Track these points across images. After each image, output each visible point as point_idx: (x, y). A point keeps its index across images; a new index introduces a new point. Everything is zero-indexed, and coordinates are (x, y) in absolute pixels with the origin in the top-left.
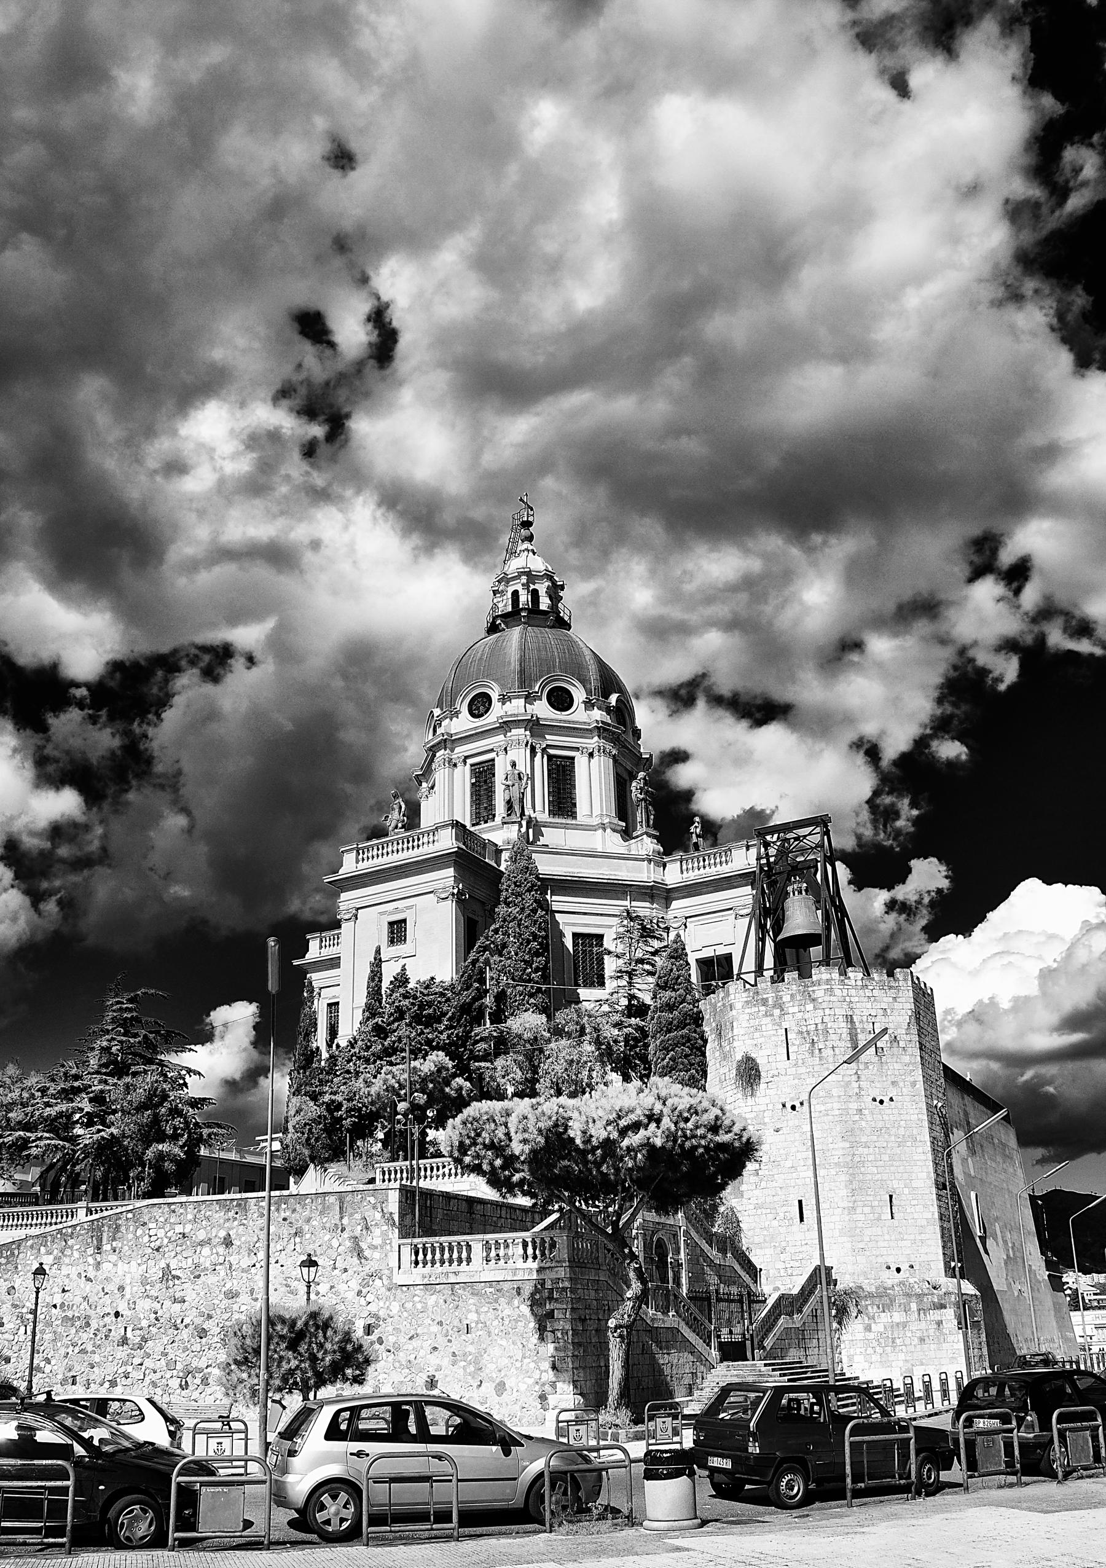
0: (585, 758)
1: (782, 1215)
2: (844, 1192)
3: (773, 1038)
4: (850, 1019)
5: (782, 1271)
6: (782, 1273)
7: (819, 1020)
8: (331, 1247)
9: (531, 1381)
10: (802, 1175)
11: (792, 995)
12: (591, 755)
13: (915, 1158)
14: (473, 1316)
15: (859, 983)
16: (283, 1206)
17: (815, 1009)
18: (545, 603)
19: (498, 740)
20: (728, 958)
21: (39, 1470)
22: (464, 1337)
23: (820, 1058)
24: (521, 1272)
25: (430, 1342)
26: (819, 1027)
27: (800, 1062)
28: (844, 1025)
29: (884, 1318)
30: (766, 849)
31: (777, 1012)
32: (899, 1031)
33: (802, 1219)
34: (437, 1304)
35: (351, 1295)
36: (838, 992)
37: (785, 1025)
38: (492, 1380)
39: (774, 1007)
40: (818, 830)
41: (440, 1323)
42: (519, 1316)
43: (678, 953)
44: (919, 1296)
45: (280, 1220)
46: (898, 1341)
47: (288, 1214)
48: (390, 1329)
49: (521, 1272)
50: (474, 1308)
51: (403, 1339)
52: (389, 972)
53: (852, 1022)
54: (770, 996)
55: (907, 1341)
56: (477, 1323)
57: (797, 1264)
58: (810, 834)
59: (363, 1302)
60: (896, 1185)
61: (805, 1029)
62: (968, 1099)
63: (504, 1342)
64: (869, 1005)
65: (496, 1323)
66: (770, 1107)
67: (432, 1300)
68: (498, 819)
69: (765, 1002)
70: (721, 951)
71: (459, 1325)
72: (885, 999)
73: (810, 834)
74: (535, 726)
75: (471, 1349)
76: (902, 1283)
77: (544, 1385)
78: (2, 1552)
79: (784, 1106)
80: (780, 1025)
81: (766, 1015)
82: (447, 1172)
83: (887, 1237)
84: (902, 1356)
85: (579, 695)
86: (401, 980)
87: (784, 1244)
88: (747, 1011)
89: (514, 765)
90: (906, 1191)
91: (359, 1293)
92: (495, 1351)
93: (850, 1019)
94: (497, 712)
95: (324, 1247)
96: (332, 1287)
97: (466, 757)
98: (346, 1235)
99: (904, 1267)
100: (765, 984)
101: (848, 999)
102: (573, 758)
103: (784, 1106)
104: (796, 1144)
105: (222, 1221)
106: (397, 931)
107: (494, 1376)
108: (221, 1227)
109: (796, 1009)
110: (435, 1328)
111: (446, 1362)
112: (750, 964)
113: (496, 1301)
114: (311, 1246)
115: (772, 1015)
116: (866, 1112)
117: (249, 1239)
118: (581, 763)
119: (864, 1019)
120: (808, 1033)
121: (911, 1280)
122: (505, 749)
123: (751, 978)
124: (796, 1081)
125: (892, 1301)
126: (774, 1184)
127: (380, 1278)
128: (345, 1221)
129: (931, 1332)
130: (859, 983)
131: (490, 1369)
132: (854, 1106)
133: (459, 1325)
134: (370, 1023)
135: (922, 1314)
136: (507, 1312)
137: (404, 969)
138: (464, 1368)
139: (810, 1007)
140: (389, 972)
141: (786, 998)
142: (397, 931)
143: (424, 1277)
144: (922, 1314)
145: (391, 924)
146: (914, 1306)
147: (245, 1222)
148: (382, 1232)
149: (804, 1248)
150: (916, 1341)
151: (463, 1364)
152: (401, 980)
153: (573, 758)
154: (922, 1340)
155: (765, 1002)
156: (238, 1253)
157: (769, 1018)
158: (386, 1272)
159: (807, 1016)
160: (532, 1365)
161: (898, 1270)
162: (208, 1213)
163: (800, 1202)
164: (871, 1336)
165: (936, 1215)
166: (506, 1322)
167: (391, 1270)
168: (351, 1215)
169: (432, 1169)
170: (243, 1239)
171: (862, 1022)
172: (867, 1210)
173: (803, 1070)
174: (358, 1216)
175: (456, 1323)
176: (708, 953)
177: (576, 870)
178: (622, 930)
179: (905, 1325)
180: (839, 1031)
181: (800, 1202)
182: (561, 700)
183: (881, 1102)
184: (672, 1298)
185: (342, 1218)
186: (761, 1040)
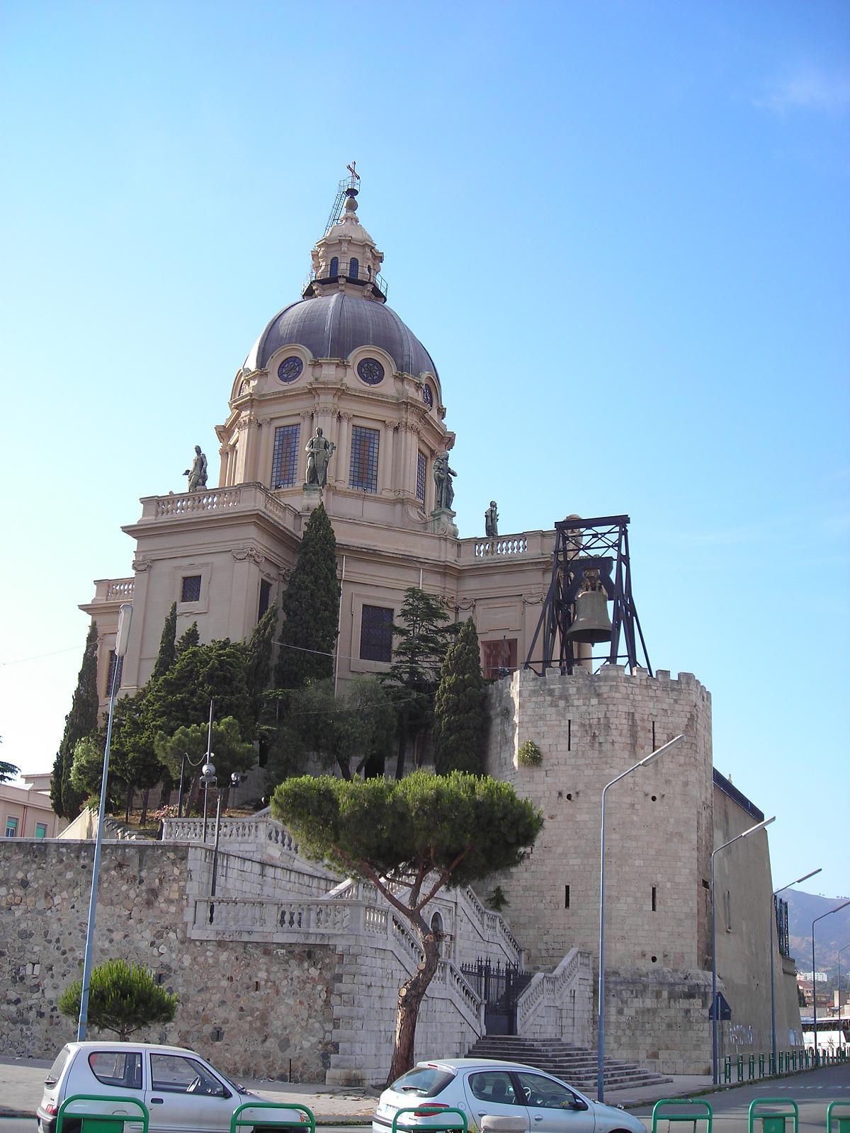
0: (390, 433)
1: (548, 898)
3: (556, 728)
4: (631, 716)
5: (543, 952)
6: (544, 953)
7: (601, 715)
8: (128, 897)
9: (314, 1040)
10: (572, 862)
11: (578, 689)
12: (396, 429)
14: (262, 975)
16: (83, 854)
17: (599, 703)
19: (303, 405)
20: (512, 644)
21: (513, 1010)
22: (253, 994)
23: (600, 752)
24: (314, 937)
25: (219, 995)
27: (580, 753)
28: (625, 721)
29: (637, 1003)
30: (564, 543)
31: (562, 703)
33: (567, 905)
34: (228, 960)
35: (144, 944)
36: (622, 690)
38: (276, 1035)
39: (561, 698)
40: (617, 529)
41: (231, 979)
42: (308, 978)
43: (470, 636)
44: (671, 985)
45: (79, 867)
46: (647, 1026)
47: (87, 861)
48: (180, 980)
49: (314, 937)
50: (264, 967)
51: (192, 991)
52: (182, 628)
53: (633, 719)
54: (557, 687)
55: (656, 1027)
56: (267, 981)
57: (558, 946)
58: (609, 532)
59: (155, 952)
62: (729, 802)
63: (291, 1002)
64: (651, 705)
65: (285, 982)
66: (547, 794)
67: (224, 956)
68: (299, 484)
69: (551, 692)
70: (510, 636)
71: (248, 981)
72: (667, 700)
73: (609, 532)
74: (342, 392)
75: (259, 1005)
76: (654, 972)
77: (327, 1044)
79: (560, 794)
80: (564, 717)
81: (551, 705)
82: (229, 832)
83: (646, 927)
84: (649, 1040)
85: (390, 369)
86: (192, 636)
87: (548, 926)
88: (534, 699)
89: (320, 432)
91: (152, 944)
92: (282, 1009)
93: (631, 716)
94: (306, 377)
95: (121, 897)
96: (126, 936)
97: (272, 419)
98: (143, 888)
99: (659, 957)
100: (554, 673)
103: (560, 794)
104: (569, 832)
105: (20, 864)
106: (191, 588)
107: (280, 1032)
108: (19, 868)
109: (580, 702)
110: (224, 983)
111: (233, 1015)
112: (538, 654)
113: (287, 962)
114: (108, 895)
115: (557, 706)
117: (46, 882)
118: (387, 438)
119: (646, 717)
120: (590, 726)
121: (665, 969)
122: (312, 415)
123: (539, 668)
124: (575, 772)
125: (645, 987)
126: (545, 868)
127: (175, 932)
128: (144, 874)
129: (679, 1020)
131: (276, 1025)
132: (628, 800)
133: (248, 981)
134: (162, 678)
136: (296, 973)
137: (195, 625)
138: (250, 1023)
139: (594, 701)
140: (182, 628)
141: (572, 690)
142: (191, 588)
143: (218, 933)
144: (672, 1002)
145: (185, 579)
146: (665, 994)
147: (44, 866)
148: (179, 887)
149: (567, 932)
150: (664, 1027)
151: (249, 1018)
152: (192, 636)
154: (670, 1026)
155: (551, 692)
156: (36, 896)
157: (554, 709)
158: (180, 925)
159: (591, 709)
160: (317, 1025)
161: (654, 959)
162: (7, 854)
163: (567, 888)
164: (623, 1019)
165: (695, 911)
166: (295, 983)
167: (186, 924)
168: (150, 868)
169: (244, 828)
170: (41, 882)
171: (643, 720)
172: (630, 900)
173: (581, 761)
174: (156, 870)
175: (246, 980)
176: (498, 636)
177: (368, 543)
178: (407, 608)
179: (653, 1011)
181: (567, 888)
182: (371, 371)
183: (654, 799)
184: (448, 970)
185: (140, 871)
186: (544, 729)
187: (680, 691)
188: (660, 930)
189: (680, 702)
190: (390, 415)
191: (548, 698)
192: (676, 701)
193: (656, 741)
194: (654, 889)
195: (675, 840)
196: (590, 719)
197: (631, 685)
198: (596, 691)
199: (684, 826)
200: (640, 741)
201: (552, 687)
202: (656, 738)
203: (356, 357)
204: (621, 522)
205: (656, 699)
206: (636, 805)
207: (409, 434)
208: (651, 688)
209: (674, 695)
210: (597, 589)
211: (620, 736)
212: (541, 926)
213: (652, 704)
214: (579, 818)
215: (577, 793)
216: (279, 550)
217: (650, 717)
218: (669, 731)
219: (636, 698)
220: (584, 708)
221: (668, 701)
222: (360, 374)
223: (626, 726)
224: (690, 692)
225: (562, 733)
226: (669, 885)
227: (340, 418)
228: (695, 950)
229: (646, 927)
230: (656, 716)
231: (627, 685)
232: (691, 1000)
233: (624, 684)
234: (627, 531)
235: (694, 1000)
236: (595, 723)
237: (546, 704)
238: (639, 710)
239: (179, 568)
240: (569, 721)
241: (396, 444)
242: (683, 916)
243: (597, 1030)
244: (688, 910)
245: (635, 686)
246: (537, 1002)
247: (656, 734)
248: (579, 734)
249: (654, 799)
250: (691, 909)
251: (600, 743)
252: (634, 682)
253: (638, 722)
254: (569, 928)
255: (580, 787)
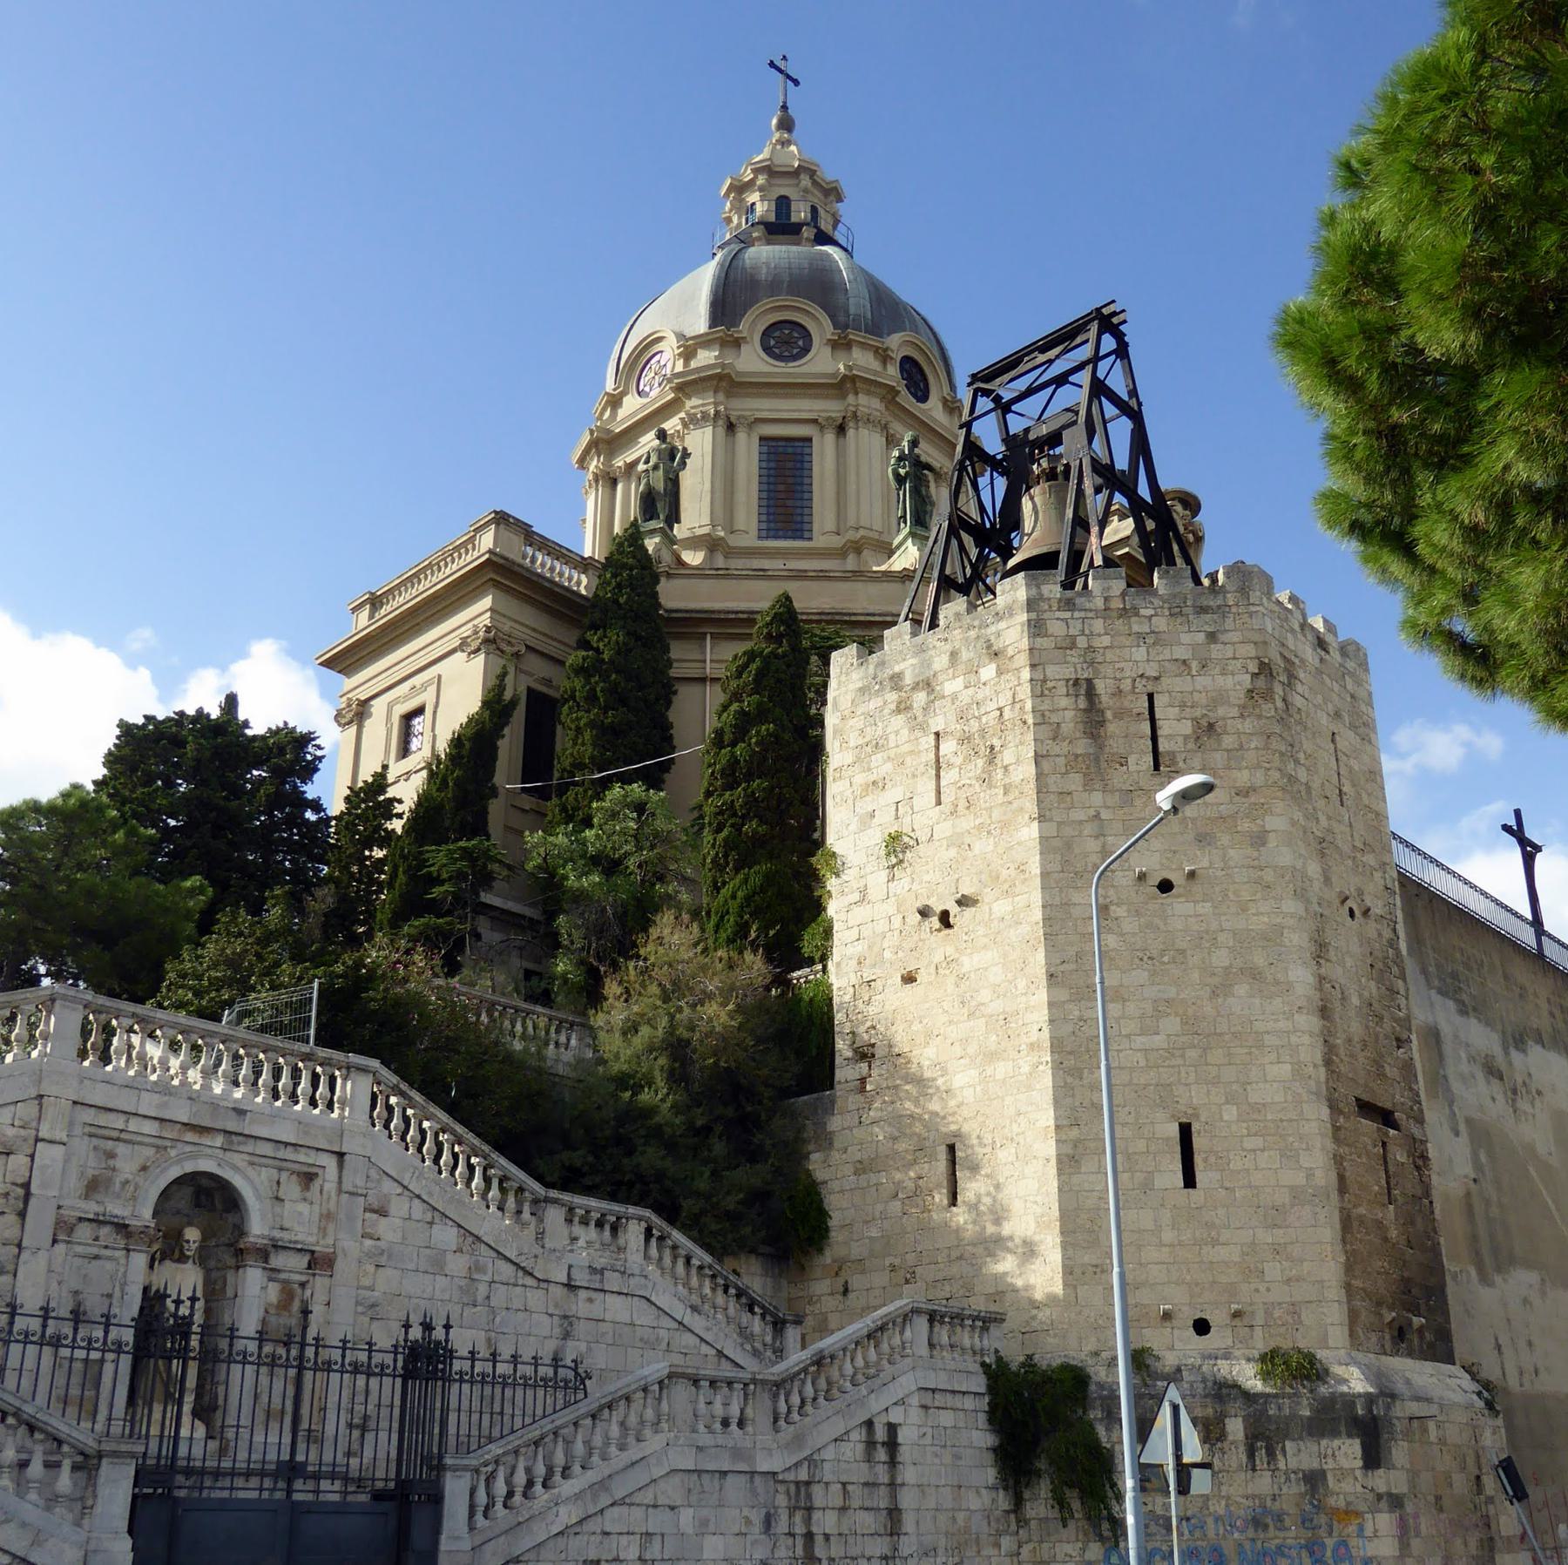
0: (830, 437)
2: (1047, 1118)
13: (1259, 1026)
15: (1117, 604)
17: (1000, 673)
18: (800, 213)
26: (1007, 714)
27: (962, 804)
28: (1064, 702)
31: (920, 698)
32: (1221, 711)
36: (1056, 628)
37: (937, 723)
39: (916, 687)
53: (1091, 693)
54: (908, 667)
60: (1196, 1098)
61: (974, 726)
64: (1140, 653)
72: (1185, 638)
78: (1338, 1559)
80: (923, 727)
81: (898, 711)
83: (1168, 1236)
85: (821, 328)
90: (1230, 1113)
99: (1216, 1318)
101: (1082, 642)
102: (810, 440)
116: (1118, 911)
118: (824, 451)
119: (1126, 685)
124: (953, 852)
130: (1117, 604)
135: (1261, 1455)
139: (988, 672)
144: (1261, 1455)
146: (1236, 1427)
153: (810, 440)
157: (899, 721)
161: (1202, 1327)
165: (1325, 1177)
171: (1119, 692)
173: (966, 823)
180: (1055, 718)
187: (1223, 611)
188: (1215, 1243)
189: (1222, 638)
190: (830, 408)
191: (892, 697)
192: (1212, 637)
193: (1160, 740)
194: (1186, 1131)
195: (1241, 990)
196: (979, 718)
197: (1077, 614)
198: (989, 647)
199: (1263, 948)
200: (1115, 745)
201: (897, 669)
202: (1159, 732)
203: (752, 325)
204: (1107, 322)
205: (1153, 639)
206: (1113, 908)
207: (864, 432)
208: (1137, 615)
209: (1208, 622)
210: (1060, 477)
211: (1054, 739)
212: (897, 1262)
213: (1143, 649)
214: (967, 963)
215: (963, 902)
216: (541, 622)
217: (1139, 684)
218: (1198, 713)
219: (1097, 643)
220: (966, 696)
221: (1189, 639)
222: (767, 349)
223: (1070, 714)
224: (1253, 609)
225: (922, 768)
226: (1230, 1113)
227: (731, 427)
228: (1335, 1292)
229: (1168, 1236)
230: (1157, 678)
231: (1067, 615)
232: (1324, 1442)
233: (1058, 614)
234: (1127, 345)
235: (1336, 1443)
236: (992, 723)
237: (886, 711)
238: (1108, 670)
239: (396, 701)
240: (937, 734)
241: (840, 454)
242: (1283, 1198)
243: (1031, 1546)
244: (1300, 1179)
245: (1090, 615)
246: (634, 1453)
247: (1159, 723)
248: (958, 760)
249: (1165, 886)
250: (1310, 1174)
251: (1006, 768)
252: (1088, 606)
253: (1104, 699)
254: (960, 1258)
255: (967, 890)
